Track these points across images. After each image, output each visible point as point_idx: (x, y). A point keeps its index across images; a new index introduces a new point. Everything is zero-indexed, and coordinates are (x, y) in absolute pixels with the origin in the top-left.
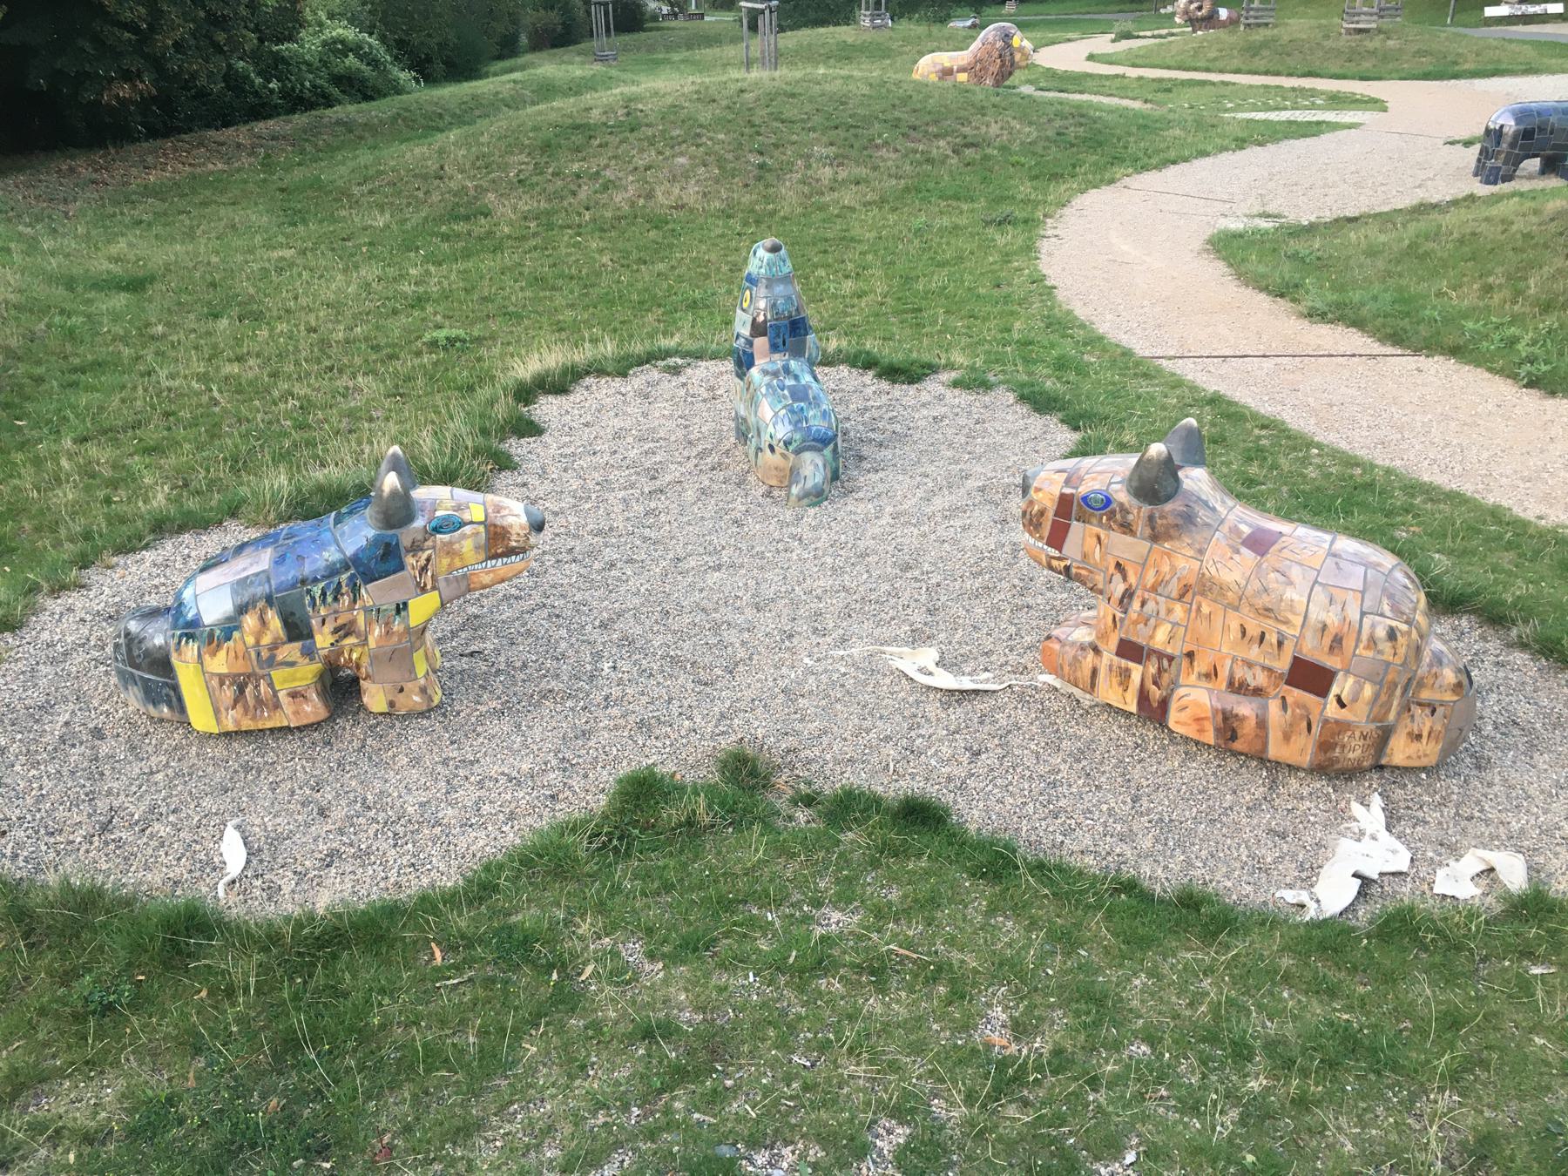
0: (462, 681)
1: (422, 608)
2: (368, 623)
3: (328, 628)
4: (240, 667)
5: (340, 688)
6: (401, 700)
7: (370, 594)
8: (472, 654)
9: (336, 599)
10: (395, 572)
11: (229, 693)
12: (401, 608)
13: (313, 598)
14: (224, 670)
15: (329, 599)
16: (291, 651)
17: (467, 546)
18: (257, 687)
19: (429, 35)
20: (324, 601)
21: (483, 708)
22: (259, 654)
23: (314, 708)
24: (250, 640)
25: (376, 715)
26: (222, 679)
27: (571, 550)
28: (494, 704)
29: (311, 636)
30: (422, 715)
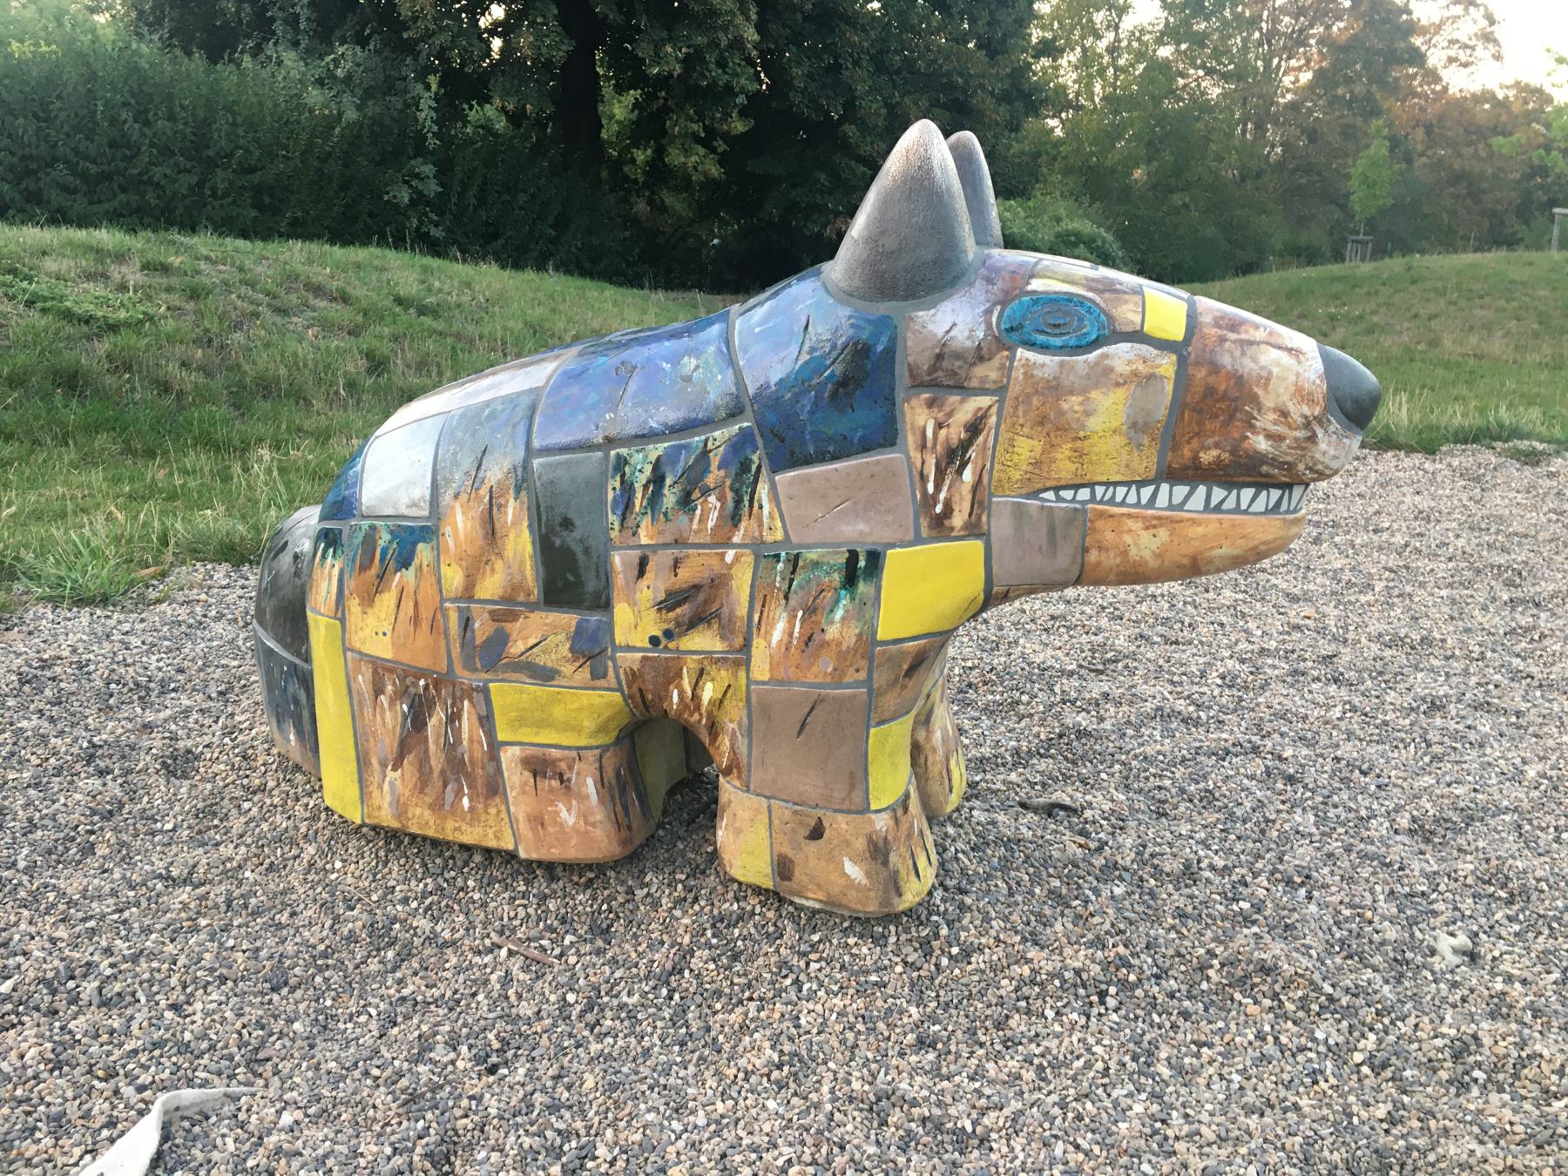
0: (1006, 866)
1: (923, 585)
2: (760, 597)
3: (651, 589)
4: (422, 652)
5: (665, 780)
6: (809, 859)
7: (790, 504)
8: (1050, 810)
9: (686, 502)
10: (866, 447)
11: (389, 719)
12: (861, 568)
13: (627, 488)
14: (383, 649)
15: (670, 498)
16: (545, 633)
17: (1107, 412)
18: (453, 718)
19: (1165, 256)
20: (654, 500)
21: (1045, 962)
22: (466, 623)
23: (580, 822)
24: (453, 577)
25: (745, 890)
26: (380, 669)
27: (1328, 659)
28: (1078, 958)
29: (603, 603)
30: (863, 925)
